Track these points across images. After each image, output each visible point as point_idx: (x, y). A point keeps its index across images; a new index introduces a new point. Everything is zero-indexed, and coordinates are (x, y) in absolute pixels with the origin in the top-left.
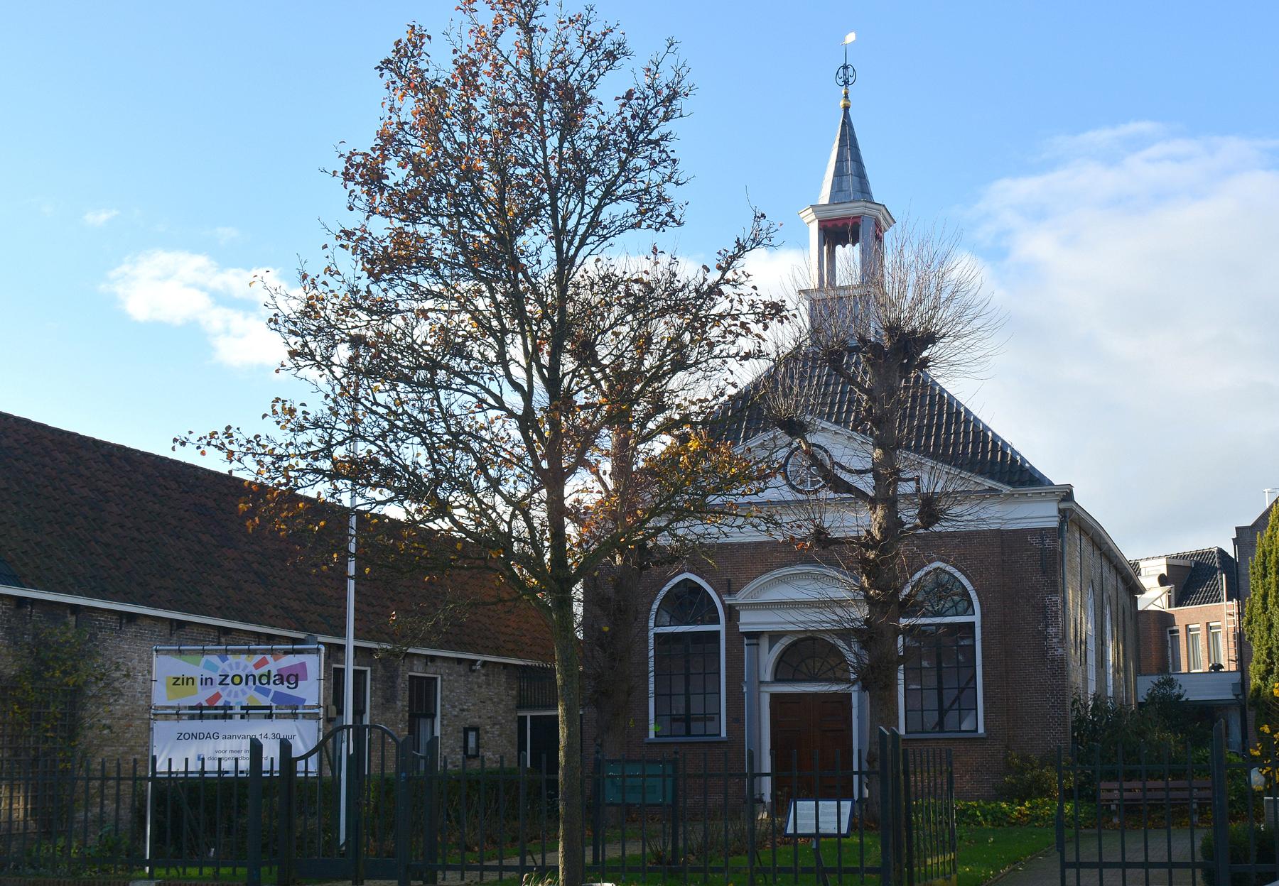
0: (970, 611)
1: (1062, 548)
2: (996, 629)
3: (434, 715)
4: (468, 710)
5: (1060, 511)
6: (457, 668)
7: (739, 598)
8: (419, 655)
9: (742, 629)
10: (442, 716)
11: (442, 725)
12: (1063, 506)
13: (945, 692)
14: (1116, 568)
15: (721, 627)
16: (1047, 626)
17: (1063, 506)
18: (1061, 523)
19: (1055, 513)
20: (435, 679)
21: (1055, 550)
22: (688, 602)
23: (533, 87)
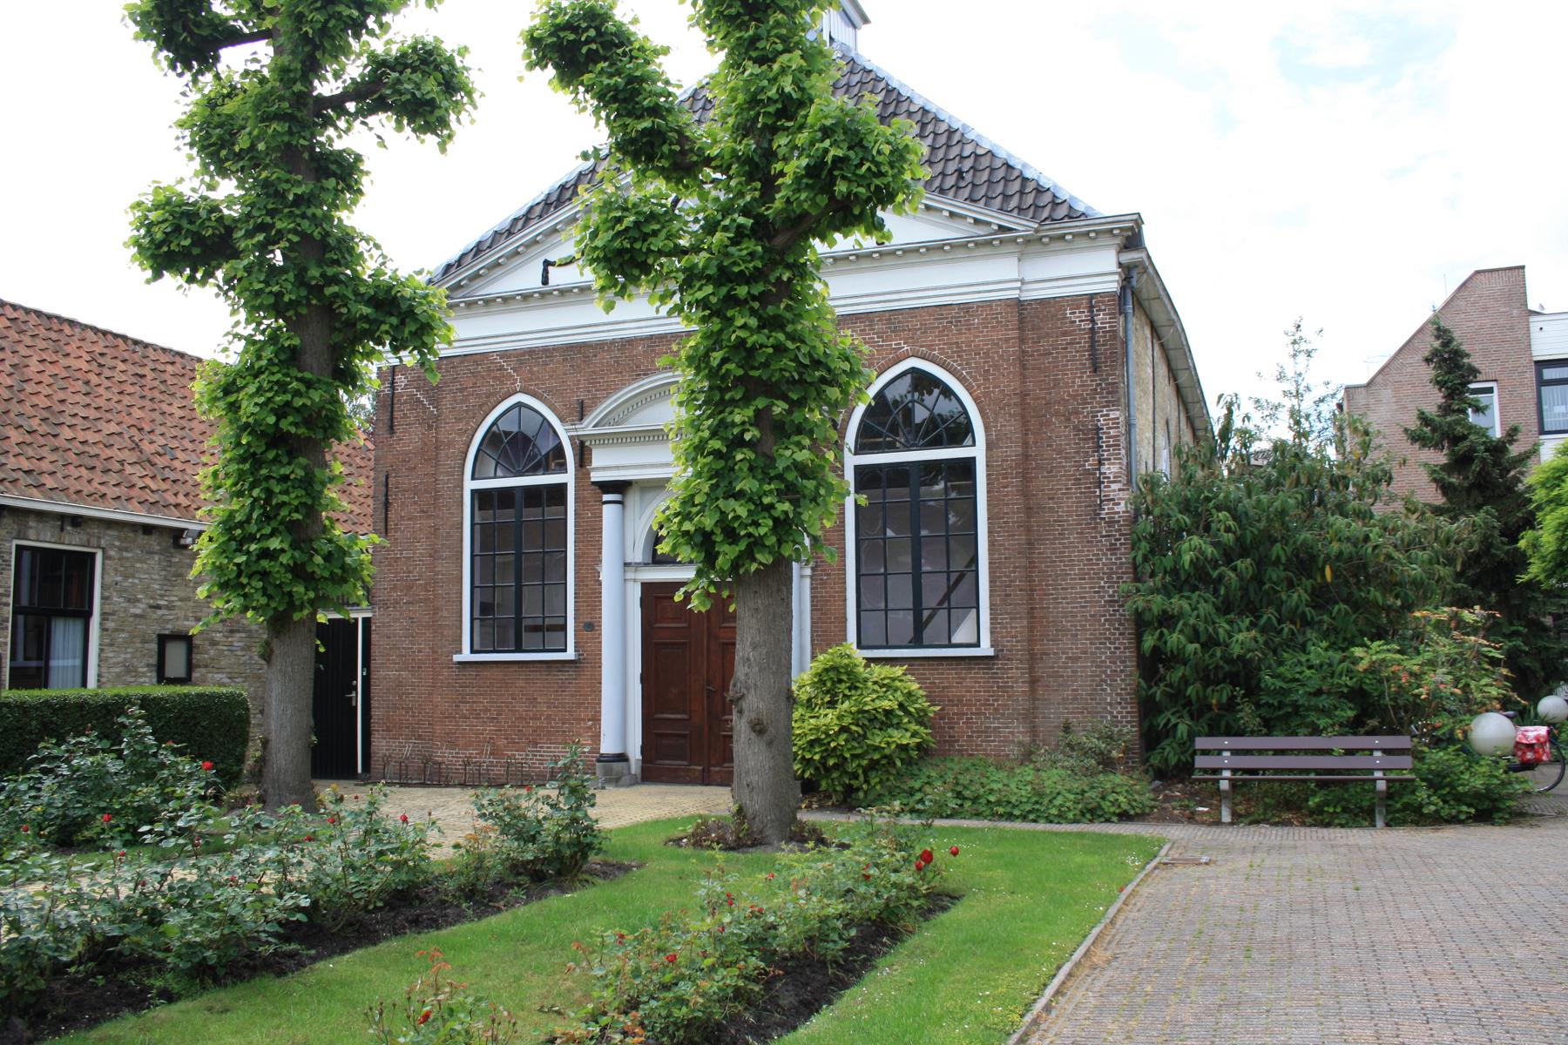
0: (968, 441)
1: (1126, 330)
2: (1022, 471)
3: (89, 614)
4: (169, 607)
5: (1120, 265)
6: (142, 539)
7: (587, 428)
8: (40, 515)
9: (596, 476)
10: (105, 616)
11: (103, 629)
12: (1128, 257)
13: (925, 579)
14: (1179, 391)
15: (568, 478)
16: (1100, 463)
17: (1128, 257)
18: (1123, 288)
19: (1114, 267)
20: (93, 555)
21: (1114, 333)
22: (513, 447)
23: (810, 939)
